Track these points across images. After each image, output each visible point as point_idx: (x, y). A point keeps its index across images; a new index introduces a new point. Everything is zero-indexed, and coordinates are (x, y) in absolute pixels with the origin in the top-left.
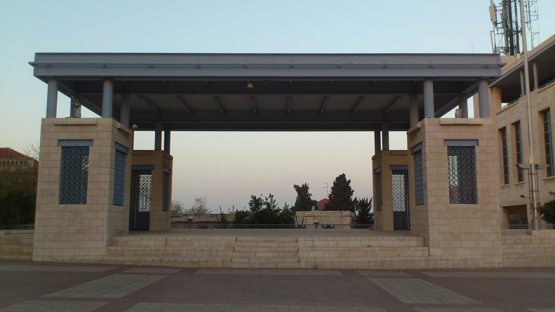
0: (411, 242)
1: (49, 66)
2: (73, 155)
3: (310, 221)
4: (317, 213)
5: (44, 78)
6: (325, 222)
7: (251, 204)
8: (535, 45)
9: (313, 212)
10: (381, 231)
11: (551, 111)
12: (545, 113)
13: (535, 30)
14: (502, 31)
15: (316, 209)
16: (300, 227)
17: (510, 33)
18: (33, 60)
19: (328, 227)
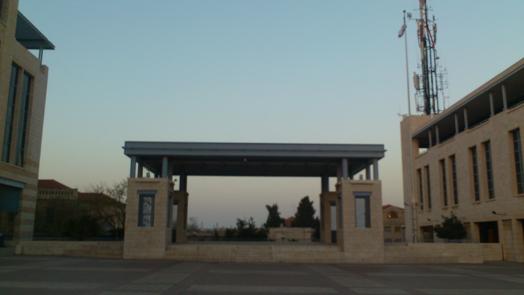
0: (335, 249)
1: (133, 149)
2: (145, 196)
3: (279, 236)
4: (285, 229)
5: (129, 156)
6: (291, 237)
7: (237, 224)
8: (447, 107)
9: (282, 228)
10: (324, 243)
11: (520, 131)
12: (515, 133)
13: (446, 95)
14: (422, 94)
15: (285, 225)
16: (271, 240)
17: (428, 96)
18: (123, 145)
19: (294, 240)
